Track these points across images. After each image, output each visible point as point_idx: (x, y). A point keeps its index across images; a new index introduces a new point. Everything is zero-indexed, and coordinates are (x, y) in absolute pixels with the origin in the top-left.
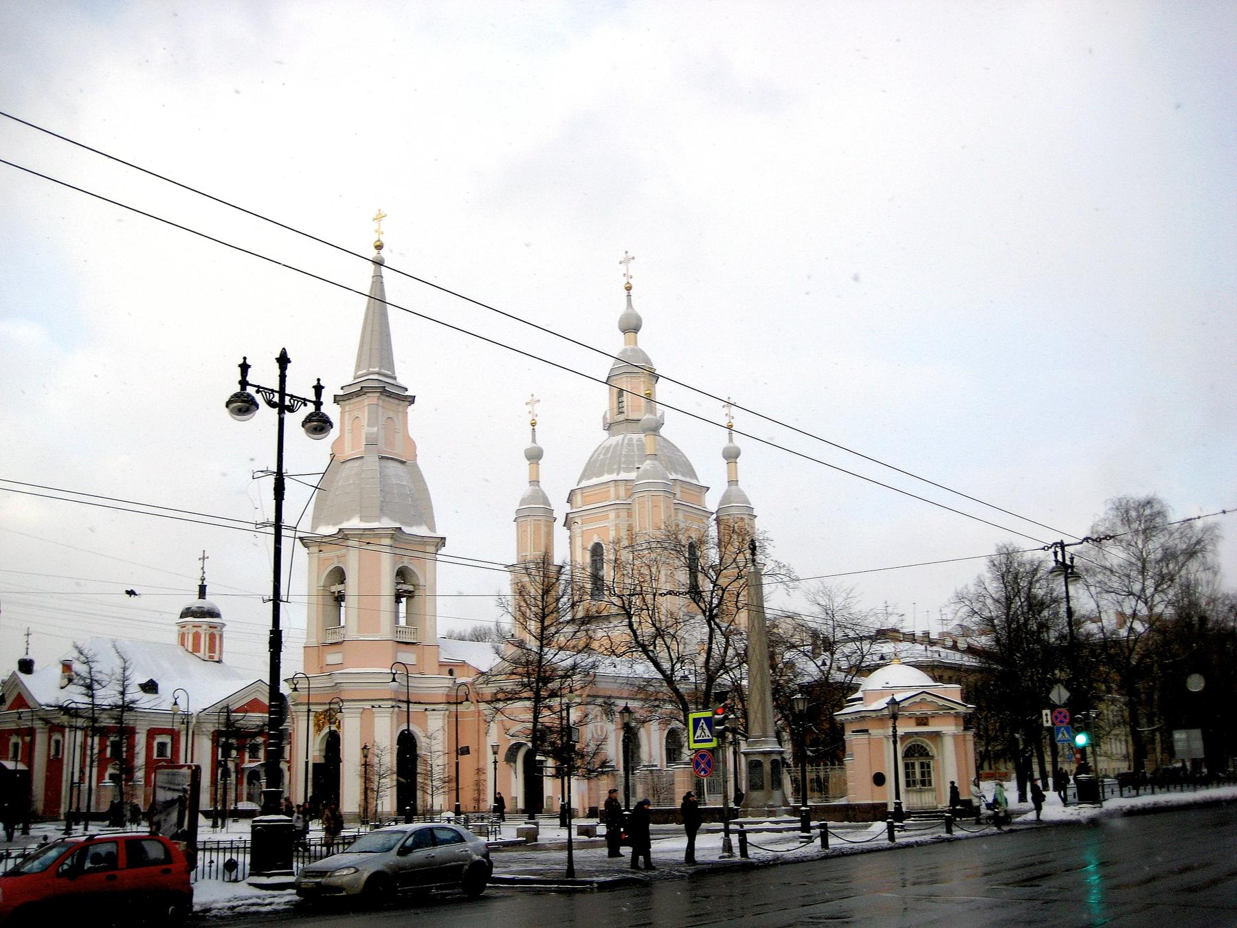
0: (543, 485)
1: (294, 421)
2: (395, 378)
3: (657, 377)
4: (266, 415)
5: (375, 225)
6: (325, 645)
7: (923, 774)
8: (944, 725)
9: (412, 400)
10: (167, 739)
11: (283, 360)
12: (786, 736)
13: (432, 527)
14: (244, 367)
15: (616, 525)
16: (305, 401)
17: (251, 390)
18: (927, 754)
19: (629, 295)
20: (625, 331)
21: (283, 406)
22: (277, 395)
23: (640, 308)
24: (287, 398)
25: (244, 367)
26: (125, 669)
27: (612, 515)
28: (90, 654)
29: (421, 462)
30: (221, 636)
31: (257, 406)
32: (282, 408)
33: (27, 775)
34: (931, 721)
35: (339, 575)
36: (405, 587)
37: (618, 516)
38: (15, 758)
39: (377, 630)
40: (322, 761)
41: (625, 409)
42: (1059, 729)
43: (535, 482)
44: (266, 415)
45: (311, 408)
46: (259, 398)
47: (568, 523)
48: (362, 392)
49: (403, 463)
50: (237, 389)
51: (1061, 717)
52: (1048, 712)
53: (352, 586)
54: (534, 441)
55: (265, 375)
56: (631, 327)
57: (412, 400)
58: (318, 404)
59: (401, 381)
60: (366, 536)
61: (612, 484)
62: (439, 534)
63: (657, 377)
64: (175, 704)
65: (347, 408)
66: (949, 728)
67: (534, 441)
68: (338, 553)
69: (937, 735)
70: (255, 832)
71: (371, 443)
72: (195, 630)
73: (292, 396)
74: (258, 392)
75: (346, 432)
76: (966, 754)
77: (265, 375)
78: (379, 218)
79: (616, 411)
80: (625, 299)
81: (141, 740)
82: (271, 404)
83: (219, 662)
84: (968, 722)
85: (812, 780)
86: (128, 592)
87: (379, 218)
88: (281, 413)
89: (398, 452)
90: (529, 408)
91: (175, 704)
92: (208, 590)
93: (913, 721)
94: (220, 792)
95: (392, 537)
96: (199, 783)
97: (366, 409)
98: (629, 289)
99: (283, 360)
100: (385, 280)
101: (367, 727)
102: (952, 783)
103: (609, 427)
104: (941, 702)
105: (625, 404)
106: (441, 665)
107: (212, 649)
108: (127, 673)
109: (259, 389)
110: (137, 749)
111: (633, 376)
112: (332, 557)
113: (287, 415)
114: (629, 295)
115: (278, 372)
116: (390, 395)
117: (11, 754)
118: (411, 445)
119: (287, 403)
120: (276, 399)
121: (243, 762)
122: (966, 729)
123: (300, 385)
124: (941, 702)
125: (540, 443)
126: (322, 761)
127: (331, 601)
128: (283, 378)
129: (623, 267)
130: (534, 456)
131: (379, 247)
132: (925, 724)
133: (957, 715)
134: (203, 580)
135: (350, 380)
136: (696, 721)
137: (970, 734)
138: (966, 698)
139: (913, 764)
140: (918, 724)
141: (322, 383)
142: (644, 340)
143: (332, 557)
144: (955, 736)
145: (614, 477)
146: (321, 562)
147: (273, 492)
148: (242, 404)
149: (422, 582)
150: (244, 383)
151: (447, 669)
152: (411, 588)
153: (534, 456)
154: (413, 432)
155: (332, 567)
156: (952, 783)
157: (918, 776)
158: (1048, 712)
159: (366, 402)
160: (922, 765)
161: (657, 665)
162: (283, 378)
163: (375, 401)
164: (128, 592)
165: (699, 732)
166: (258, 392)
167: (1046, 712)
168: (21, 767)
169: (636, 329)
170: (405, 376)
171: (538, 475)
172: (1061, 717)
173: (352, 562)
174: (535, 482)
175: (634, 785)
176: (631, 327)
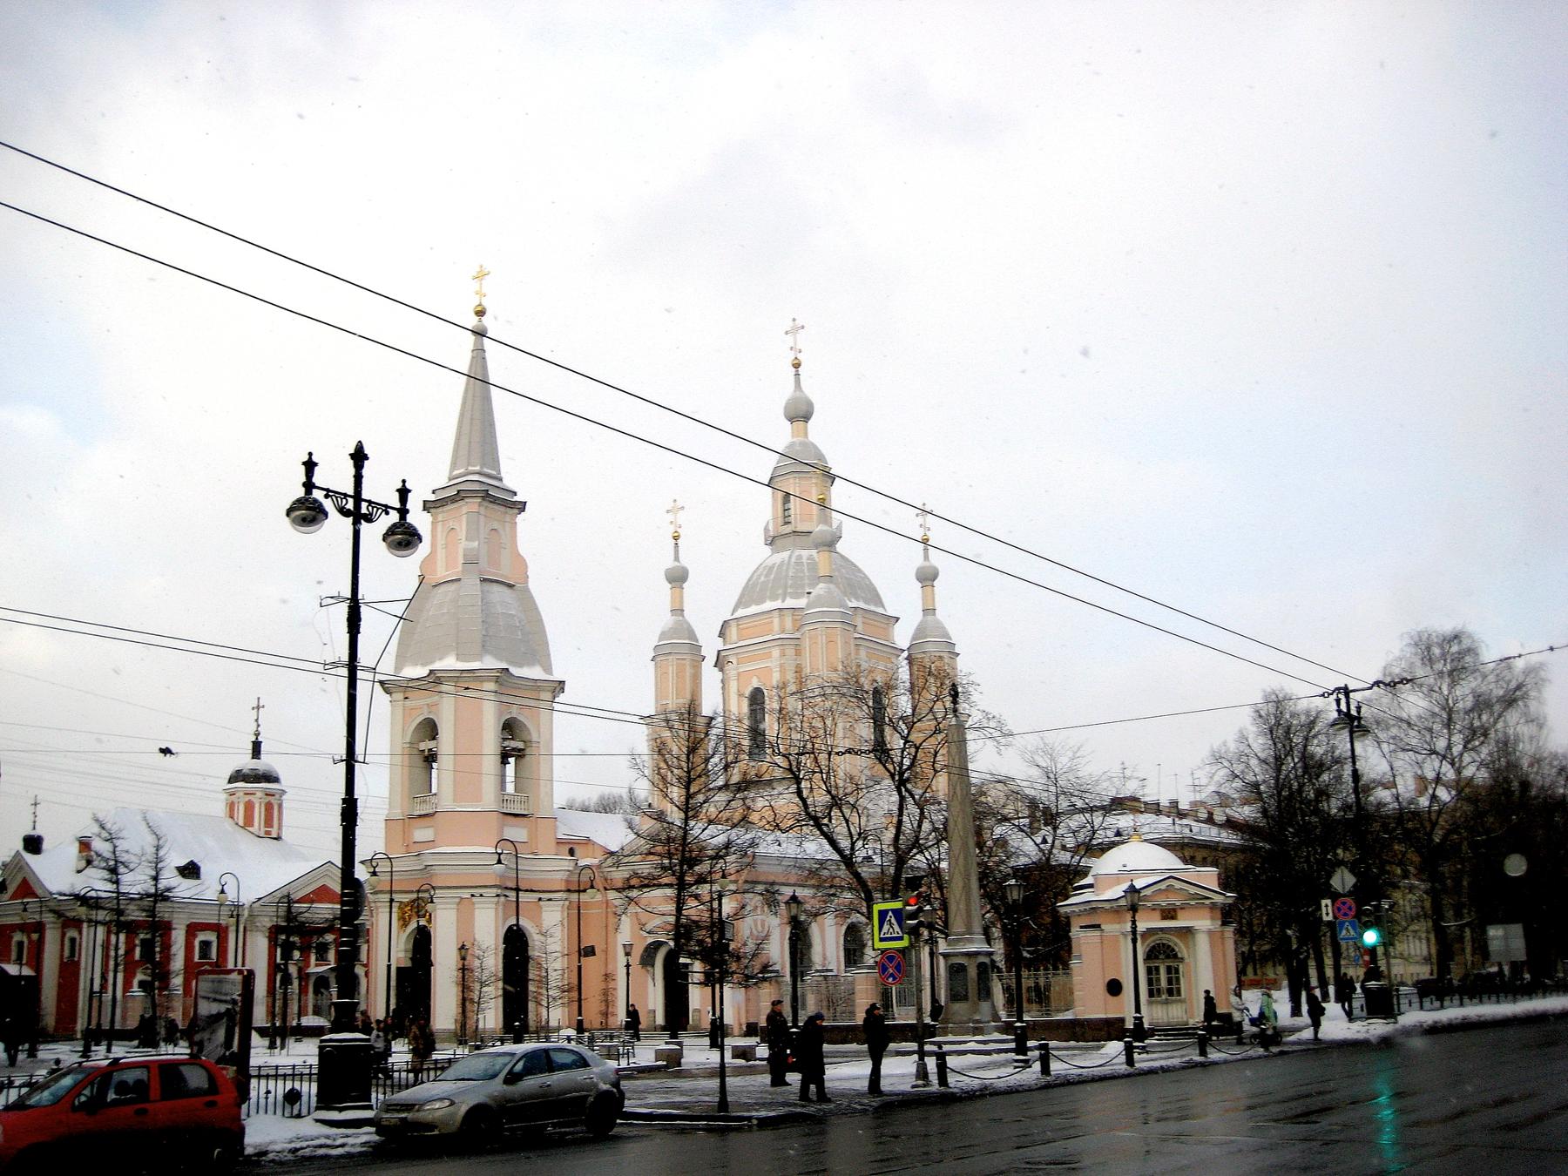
0: (689, 615)
1: (372, 533)
2: (501, 480)
3: (833, 478)
4: (337, 527)
5: (475, 285)
6: (412, 817)
7: (1170, 981)
8: (1197, 919)
9: (522, 507)
10: (211, 937)
11: (359, 457)
12: (996, 932)
13: (548, 668)
14: (310, 466)
15: (781, 666)
16: (386, 509)
17: (318, 495)
18: (1175, 956)
19: (797, 374)
20: (792, 419)
21: (358, 515)
22: (351, 501)
23: (811, 390)
24: (364, 505)
25: (310, 466)
26: (158, 848)
27: (776, 652)
28: (114, 829)
29: (534, 586)
30: (280, 806)
31: (326, 515)
32: (358, 517)
33: (35, 982)
34: (1180, 914)
35: (430, 729)
36: (514, 744)
37: (783, 654)
38: (19, 961)
39: (478, 798)
40: (409, 964)
41: (792, 519)
42: (1342, 924)
43: (678, 611)
44: (337, 527)
45: (394, 517)
46: (328, 505)
47: (720, 663)
48: (459, 497)
49: (511, 586)
50: (301, 492)
51: (1344, 909)
52: (1329, 902)
53: (446, 743)
54: (677, 558)
55: (335, 475)
56: (800, 414)
57: (522, 507)
58: (403, 512)
59: (508, 483)
60: (464, 680)
61: (776, 614)
62: (557, 676)
63: (833, 478)
64: (222, 892)
65: (440, 518)
66: (1203, 923)
67: (677, 558)
68: (429, 701)
69: (1188, 931)
70: (323, 1054)
71: (471, 561)
72: (248, 798)
73: (370, 502)
74: (327, 496)
75: (439, 547)
76: (1224, 956)
77: (335, 475)
78: (481, 276)
79: (780, 521)
80: (792, 378)
81: (178, 937)
82: (344, 512)
83: (278, 838)
84: (1227, 915)
85: (1029, 989)
86: (162, 751)
87: (481, 276)
88: (356, 523)
89: (505, 573)
90: (670, 517)
91: (222, 892)
92: (263, 748)
93: (1157, 914)
94: (278, 1004)
95: (497, 680)
96: (252, 992)
97: (464, 519)
98: (797, 366)
99: (359, 457)
100: (487, 355)
101: (465, 922)
102: (1207, 992)
103: (772, 541)
104: (1193, 890)
105: (792, 512)
106: (560, 842)
107: (268, 822)
108: (161, 853)
109: (328, 493)
110: (174, 950)
111: (803, 477)
112: (421, 706)
113: (364, 526)
114: (797, 374)
115: (352, 471)
116: (495, 500)
117: (14, 956)
118: (521, 564)
119: (364, 511)
120: (350, 505)
121: (308, 965)
122: (1224, 924)
123: (380, 488)
124: (1193, 890)
125: (685, 561)
126: (409, 964)
127: (419, 761)
128: (358, 479)
129: (790, 338)
130: (677, 578)
131: (480, 313)
132: (1173, 918)
133: (1213, 906)
134: (257, 735)
135: (444, 482)
136: (883, 914)
137: (1230, 930)
138: (1225, 884)
139: (1157, 969)
140: (1164, 918)
141: (408, 486)
142: (816, 430)
143: (421, 706)
144: (1210, 933)
145: (778, 604)
146: (407, 713)
147: (346, 624)
148: (307, 512)
149: (535, 737)
150: (309, 486)
151: (567, 848)
152: (520, 745)
153: (677, 578)
154: (524, 547)
155: (421, 718)
156: (1207, 992)
157: (1164, 984)
158: (1329, 902)
159: (465, 510)
160: (1169, 970)
161: (833, 843)
162: (358, 479)
163: (475, 508)
164: (162, 751)
165: (886, 927)
166: (327, 496)
167: (1326, 902)
168: (27, 971)
169: (806, 418)
170: (513, 477)
171: (682, 602)
172: (1344, 909)
173: (446, 713)
174: (678, 611)
175: (804, 995)
176: (800, 414)
